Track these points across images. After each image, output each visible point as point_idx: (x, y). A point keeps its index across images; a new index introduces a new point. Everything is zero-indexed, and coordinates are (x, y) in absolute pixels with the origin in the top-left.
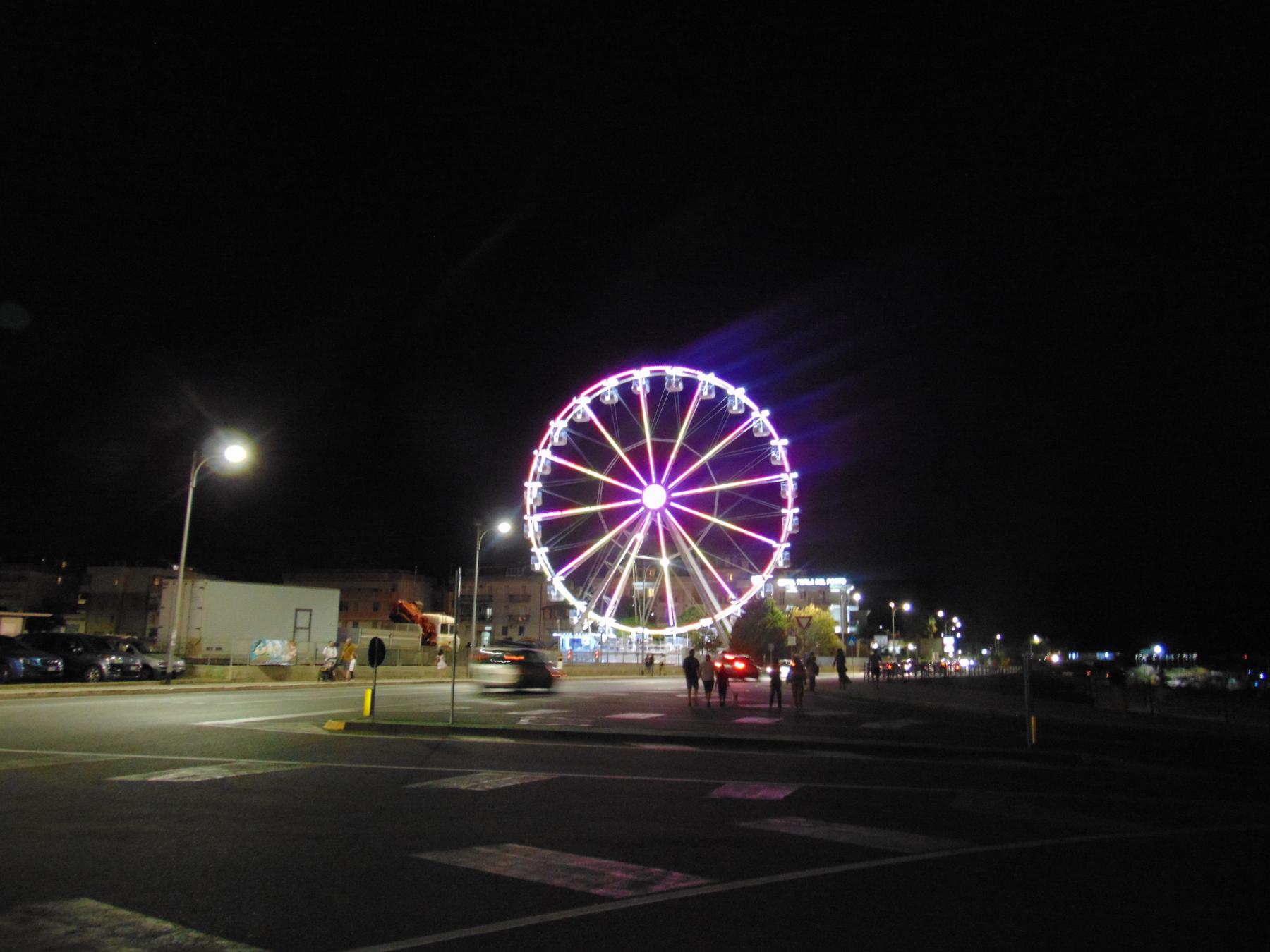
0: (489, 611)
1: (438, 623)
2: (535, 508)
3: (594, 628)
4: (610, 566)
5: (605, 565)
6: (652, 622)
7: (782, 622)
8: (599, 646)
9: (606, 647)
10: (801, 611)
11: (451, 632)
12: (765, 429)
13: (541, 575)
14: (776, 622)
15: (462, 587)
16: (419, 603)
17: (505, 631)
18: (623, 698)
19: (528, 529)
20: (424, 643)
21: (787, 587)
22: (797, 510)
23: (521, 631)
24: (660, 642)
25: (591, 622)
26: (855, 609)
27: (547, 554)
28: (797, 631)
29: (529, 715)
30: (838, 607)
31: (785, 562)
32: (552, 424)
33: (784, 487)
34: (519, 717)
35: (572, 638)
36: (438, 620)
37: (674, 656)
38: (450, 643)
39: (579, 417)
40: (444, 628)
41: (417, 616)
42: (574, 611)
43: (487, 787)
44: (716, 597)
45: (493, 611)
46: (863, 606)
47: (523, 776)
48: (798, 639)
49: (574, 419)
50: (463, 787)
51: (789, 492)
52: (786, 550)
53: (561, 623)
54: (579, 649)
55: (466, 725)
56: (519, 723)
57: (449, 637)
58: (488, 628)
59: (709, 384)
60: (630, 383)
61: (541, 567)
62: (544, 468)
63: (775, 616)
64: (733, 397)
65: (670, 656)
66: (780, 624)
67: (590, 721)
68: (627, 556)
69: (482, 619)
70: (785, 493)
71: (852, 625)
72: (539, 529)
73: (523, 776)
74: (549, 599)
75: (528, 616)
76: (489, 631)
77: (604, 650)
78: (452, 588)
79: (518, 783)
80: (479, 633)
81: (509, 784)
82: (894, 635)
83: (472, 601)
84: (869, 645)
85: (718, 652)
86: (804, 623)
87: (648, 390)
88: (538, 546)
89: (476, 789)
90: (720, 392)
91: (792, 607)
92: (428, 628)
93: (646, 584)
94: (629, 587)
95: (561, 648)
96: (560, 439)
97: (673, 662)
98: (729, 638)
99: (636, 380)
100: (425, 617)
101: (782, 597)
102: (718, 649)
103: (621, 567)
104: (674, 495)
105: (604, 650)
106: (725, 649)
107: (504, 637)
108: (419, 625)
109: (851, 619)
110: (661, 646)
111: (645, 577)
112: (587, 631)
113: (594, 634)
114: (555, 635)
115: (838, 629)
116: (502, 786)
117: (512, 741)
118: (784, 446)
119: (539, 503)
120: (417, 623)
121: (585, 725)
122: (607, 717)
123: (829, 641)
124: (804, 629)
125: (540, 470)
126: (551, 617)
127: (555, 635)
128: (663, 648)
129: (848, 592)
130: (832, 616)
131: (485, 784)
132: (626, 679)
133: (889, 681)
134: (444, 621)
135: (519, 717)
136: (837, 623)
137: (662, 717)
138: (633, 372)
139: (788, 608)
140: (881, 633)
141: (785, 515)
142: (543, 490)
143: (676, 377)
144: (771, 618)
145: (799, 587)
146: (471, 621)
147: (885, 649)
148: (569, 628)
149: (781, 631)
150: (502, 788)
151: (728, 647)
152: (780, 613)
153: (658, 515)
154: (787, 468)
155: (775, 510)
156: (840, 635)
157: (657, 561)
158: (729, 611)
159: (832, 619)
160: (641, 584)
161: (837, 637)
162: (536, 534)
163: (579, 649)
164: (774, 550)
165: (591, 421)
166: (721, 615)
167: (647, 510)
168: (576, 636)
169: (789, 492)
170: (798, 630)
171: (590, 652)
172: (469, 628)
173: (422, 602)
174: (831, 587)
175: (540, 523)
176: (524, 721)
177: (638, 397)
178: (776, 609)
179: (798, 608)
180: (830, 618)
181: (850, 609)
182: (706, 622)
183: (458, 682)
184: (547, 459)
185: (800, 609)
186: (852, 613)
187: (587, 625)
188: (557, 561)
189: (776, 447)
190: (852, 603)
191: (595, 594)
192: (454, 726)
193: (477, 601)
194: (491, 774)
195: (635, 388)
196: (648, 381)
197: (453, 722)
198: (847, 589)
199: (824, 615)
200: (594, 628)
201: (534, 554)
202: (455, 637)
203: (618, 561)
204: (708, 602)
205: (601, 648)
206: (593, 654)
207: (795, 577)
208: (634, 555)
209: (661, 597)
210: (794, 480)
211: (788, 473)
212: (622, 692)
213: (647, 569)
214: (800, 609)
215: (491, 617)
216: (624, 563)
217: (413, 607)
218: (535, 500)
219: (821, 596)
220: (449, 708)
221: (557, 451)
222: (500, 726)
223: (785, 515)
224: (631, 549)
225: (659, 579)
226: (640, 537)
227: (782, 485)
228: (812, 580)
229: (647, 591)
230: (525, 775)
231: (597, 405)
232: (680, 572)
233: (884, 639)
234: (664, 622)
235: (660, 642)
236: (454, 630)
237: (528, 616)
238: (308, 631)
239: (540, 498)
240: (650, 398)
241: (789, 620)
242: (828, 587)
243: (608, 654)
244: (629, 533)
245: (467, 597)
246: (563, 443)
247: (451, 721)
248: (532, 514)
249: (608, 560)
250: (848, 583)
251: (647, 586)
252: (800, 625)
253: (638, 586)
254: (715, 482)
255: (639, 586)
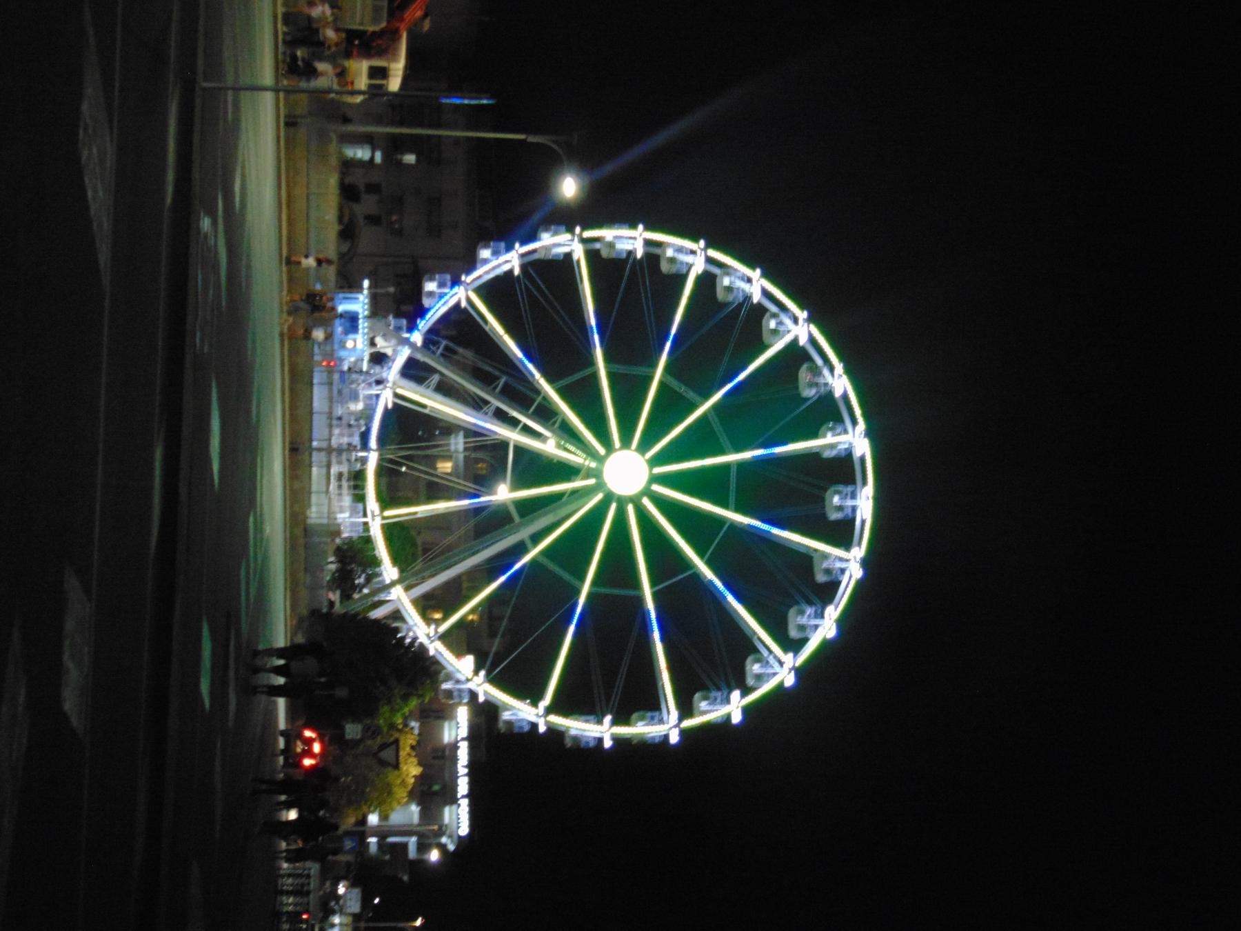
0: (410, 158)
1: (389, 61)
2: (598, 246)
3: (379, 359)
4: (495, 388)
5: (498, 378)
6: (387, 472)
7: (387, 715)
8: (346, 368)
9: (342, 380)
10: (408, 749)
11: (371, 86)
12: (759, 678)
13: (471, 263)
14: (389, 702)
15: (457, 107)
16: (427, 25)
17: (373, 188)
18: (248, 411)
19: (556, 233)
20: (351, 35)
21: (453, 723)
22: (608, 744)
23: (373, 220)
24: (352, 483)
25: (389, 352)
26: (412, 853)
27: (511, 272)
28: (369, 742)
29: (216, 232)
30: (416, 819)
31: (509, 723)
32: (756, 274)
33: (652, 718)
34: (212, 213)
35: (360, 316)
36: (395, 58)
37: (325, 510)
38: (352, 83)
39: (773, 324)
40: (379, 73)
41: (402, 20)
42: (449, 283)
43: (85, 153)
44: (434, 589)
45: (409, 166)
46: (419, 866)
47: (105, 219)
48: (357, 743)
49: (768, 314)
50: (85, 107)
51: (641, 729)
52: (534, 726)
53: (388, 294)
54: (339, 329)
55: (197, 128)
56: (202, 214)
57: (362, 82)
58: (378, 157)
59: (843, 571)
60: (839, 420)
61: (485, 261)
62: (672, 260)
63: (399, 701)
64: (821, 615)
65: (326, 502)
66: (385, 709)
67: (206, 350)
68: (513, 423)
69: (394, 146)
70: (642, 719)
71: (381, 845)
72: (558, 255)
73: (105, 219)
74: (426, 277)
75: (400, 233)
76: (372, 158)
77: (336, 376)
78: (455, 88)
79: (92, 212)
80: (368, 140)
81: (90, 194)
82: (362, 925)
83: (430, 126)
84: (344, 878)
85: (334, 591)
86: (387, 754)
87: (828, 454)
88: (523, 256)
89: (81, 132)
90: (827, 592)
91: (416, 731)
92: (380, 42)
93: (461, 457)
94: (449, 428)
95: (341, 295)
96: (729, 289)
97: (314, 509)
98: (357, 614)
99: (846, 432)
100: (400, 37)
101: (437, 712)
102: (338, 593)
103: (493, 408)
104: (657, 488)
105: (336, 376)
106: (337, 605)
107: (362, 188)
108: (384, 25)
109: (394, 845)
110: (345, 484)
111: (474, 455)
112: (372, 343)
113: (366, 358)
114: (366, 283)
115: (373, 819)
116: (87, 180)
117: (169, 200)
118: (729, 717)
119: (605, 253)
120: (388, 22)
121: (200, 341)
122: (214, 384)
123: (350, 803)
124: (375, 755)
125: (670, 253)
126: (397, 276)
127: (366, 283)
128: (340, 487)
129: (444, 840)
130: (398, 808)
131: (90, 149)
132: (284, 416)
133: (277, 915)
134: (392, 73)
135: (212, 213)
136: (384, 817)
137: (213, 485)
138: (861, 426)
139: (414, 724)
140: (366, 901)
141: (600, 722)
142: (631, 261)
143: (854, 509)
144: (396, 691)
145: (454, 747)
146: (392, 123)
147: (336, 907)
148: (378, 309)
149: (372, 712)
150: (82, 188)
151: (343, 611)
152: (406, 710)
153: (592, 481)
154: (688, 723)
155: (608, 699)
156: (363, 821)
157: (505, 477)
158: (412, 615)
159: (393, 810)
160: (461, 447)
161: (360, 817)
162: (547, 248)
163: (339, 329)
164: (535, 704)
165: (764, 347)
166: (400, 598)
167: (601, 460)
168: (363, 324)
169: (641, 729)
170: (374, 744)
171: (333, 350)
172: (379, 121)
173: (431, 28)
174: (454, 807)
175: (568, 256)
176: (206, 223)
177: (814, 435)
178: (414, 703)
179: (414, 743)
180: (395, 804)
181: (413, 840)
182: (389, 572)
183: (277, 99)
184: (690, 266)
185: (413, 747)
186: (404, 846)
187: (382, 345)
188: (497, 290)
189: (727, 701)
190: (423, 847)
191: (442, 359)
192: (197, 89)
193: (429, 137)
194: (108, 164)
195: (832, 429)
196: (843, 454)
197: (204, 89)
198: (450, 836)
199: (402, 793)
200: (379, 359)
201: (509, 248)
202: (360, 92)
203: (503, 402)
204: (427, 573)
205: (342, 373)
206: (330, 356)
207: (472, 738)
208: (513, 436)
209: (434, 491)
210: (666, 737)
211: (677, 726)
212: (258, 413)
213: (488, 459)
214: (413, 747)
215: (399, 163)
216: (501, 416)
217: (419, 14)
218: (611, 245)
219: (436, 788)
220: (230, 80)
221: (707, 282)
222: (196, 175)
223: (600, 722)
224: (527, 430)
225: (470, 486)
226: (550, 446)
227: (657, 714)
228: (466, 771)
229: (448, 457)
230: (106, 225)
231: (795, 356)
232: (494, 520)
233: (354, 906)
234: (388, 499)
235: (352, 483)
236: (376, 91)
237: (400, 233)
238: (242, 93)
239: (613, 255)
240: (805, 561)
241: (392, 726)
242: (453, 800)
243: (330, 384)
244: (557, 425)
245: (436, 116)
246: (720, 295)
247: (205, 85)
248: (584, 241)
249: (506, 385)
250: (460, 837)
251: (457, 458)
252: (384, 746)
253: (458, 443)
254: (657, 588)
255: (456, 444)
